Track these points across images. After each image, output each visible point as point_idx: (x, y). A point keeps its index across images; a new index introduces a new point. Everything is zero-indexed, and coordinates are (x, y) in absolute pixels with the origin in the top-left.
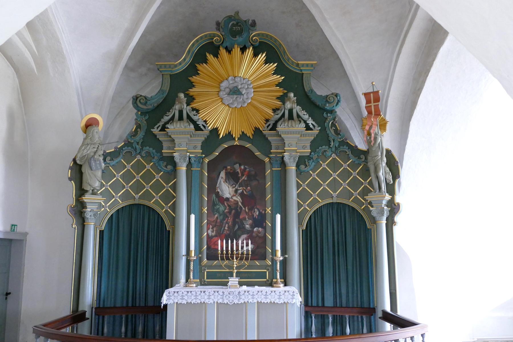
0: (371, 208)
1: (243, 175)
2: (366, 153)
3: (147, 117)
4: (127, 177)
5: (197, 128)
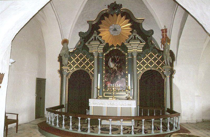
0: (164, 72)
1: (118, 60)
2: (162, 51)
3: (84, 39)
4: (77, 60)
5: (101, 43)
